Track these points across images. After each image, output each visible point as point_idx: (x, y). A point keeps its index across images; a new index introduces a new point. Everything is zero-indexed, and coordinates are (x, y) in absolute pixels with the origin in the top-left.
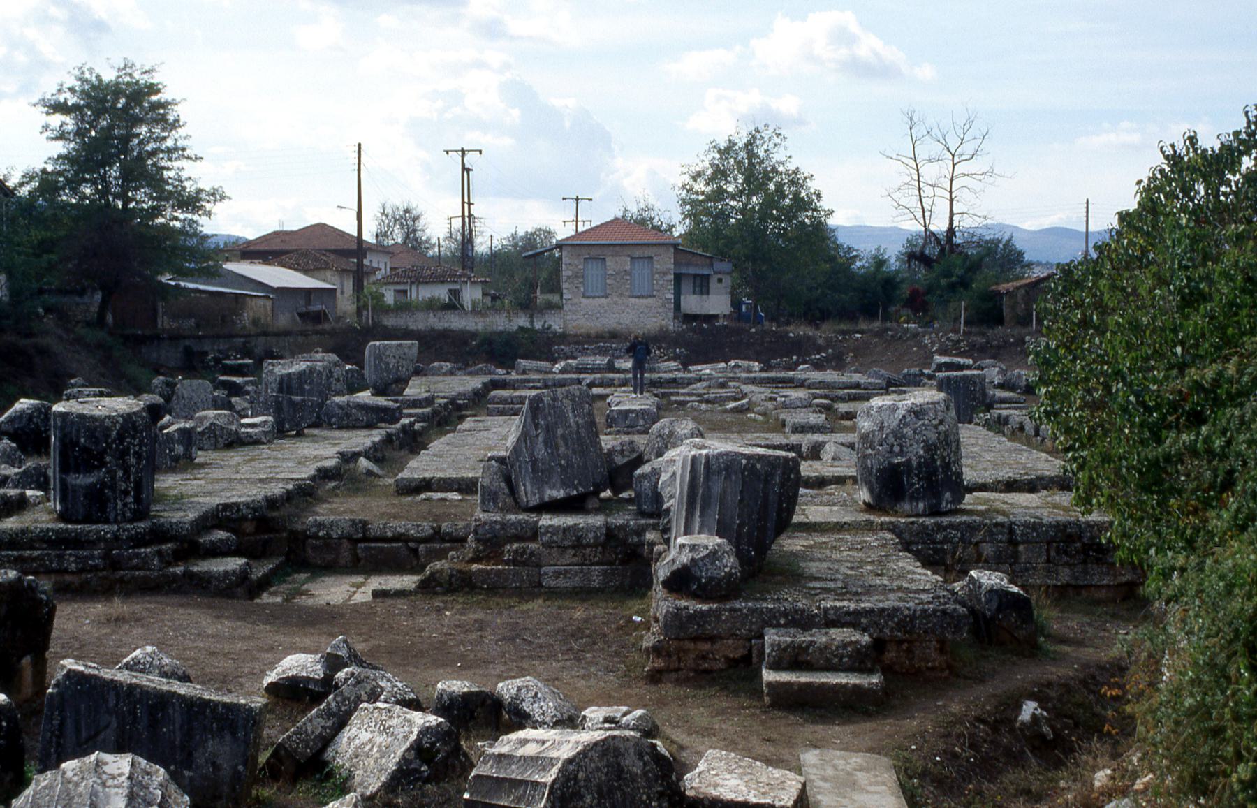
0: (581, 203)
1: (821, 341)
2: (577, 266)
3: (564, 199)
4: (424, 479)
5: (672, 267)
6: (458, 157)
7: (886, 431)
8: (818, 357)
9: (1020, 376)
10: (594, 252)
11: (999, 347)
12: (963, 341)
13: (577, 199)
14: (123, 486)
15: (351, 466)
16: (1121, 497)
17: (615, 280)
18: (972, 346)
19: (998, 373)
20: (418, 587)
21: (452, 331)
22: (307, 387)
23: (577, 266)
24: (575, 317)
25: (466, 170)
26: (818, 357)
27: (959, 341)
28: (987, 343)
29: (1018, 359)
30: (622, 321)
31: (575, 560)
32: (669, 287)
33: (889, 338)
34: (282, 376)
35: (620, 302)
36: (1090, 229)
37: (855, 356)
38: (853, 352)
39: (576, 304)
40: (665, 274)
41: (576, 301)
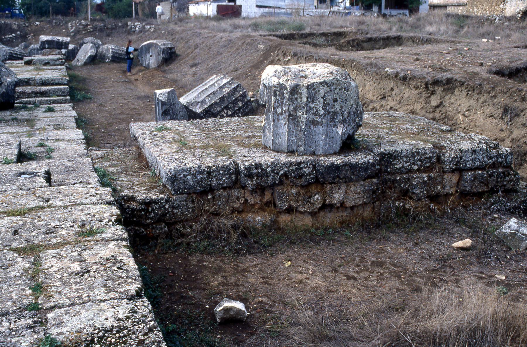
1: (15, 27)
7: (460, 89)
8: (10, 36)
9: (108, 50)
11: (112, 29)
12: (89, 25)
15: (123, 126)
16: (360, 171)
18: (95, 28)
19: (92, 48)
20: (213, 312)
21: (230, 18)
26: (10, 36)
27: (87, 25)
28: (105, 26)
29: (123, 36)
33: (54, 24)
34: (164, 49)
37: (34, 36)
38: (33, 33)
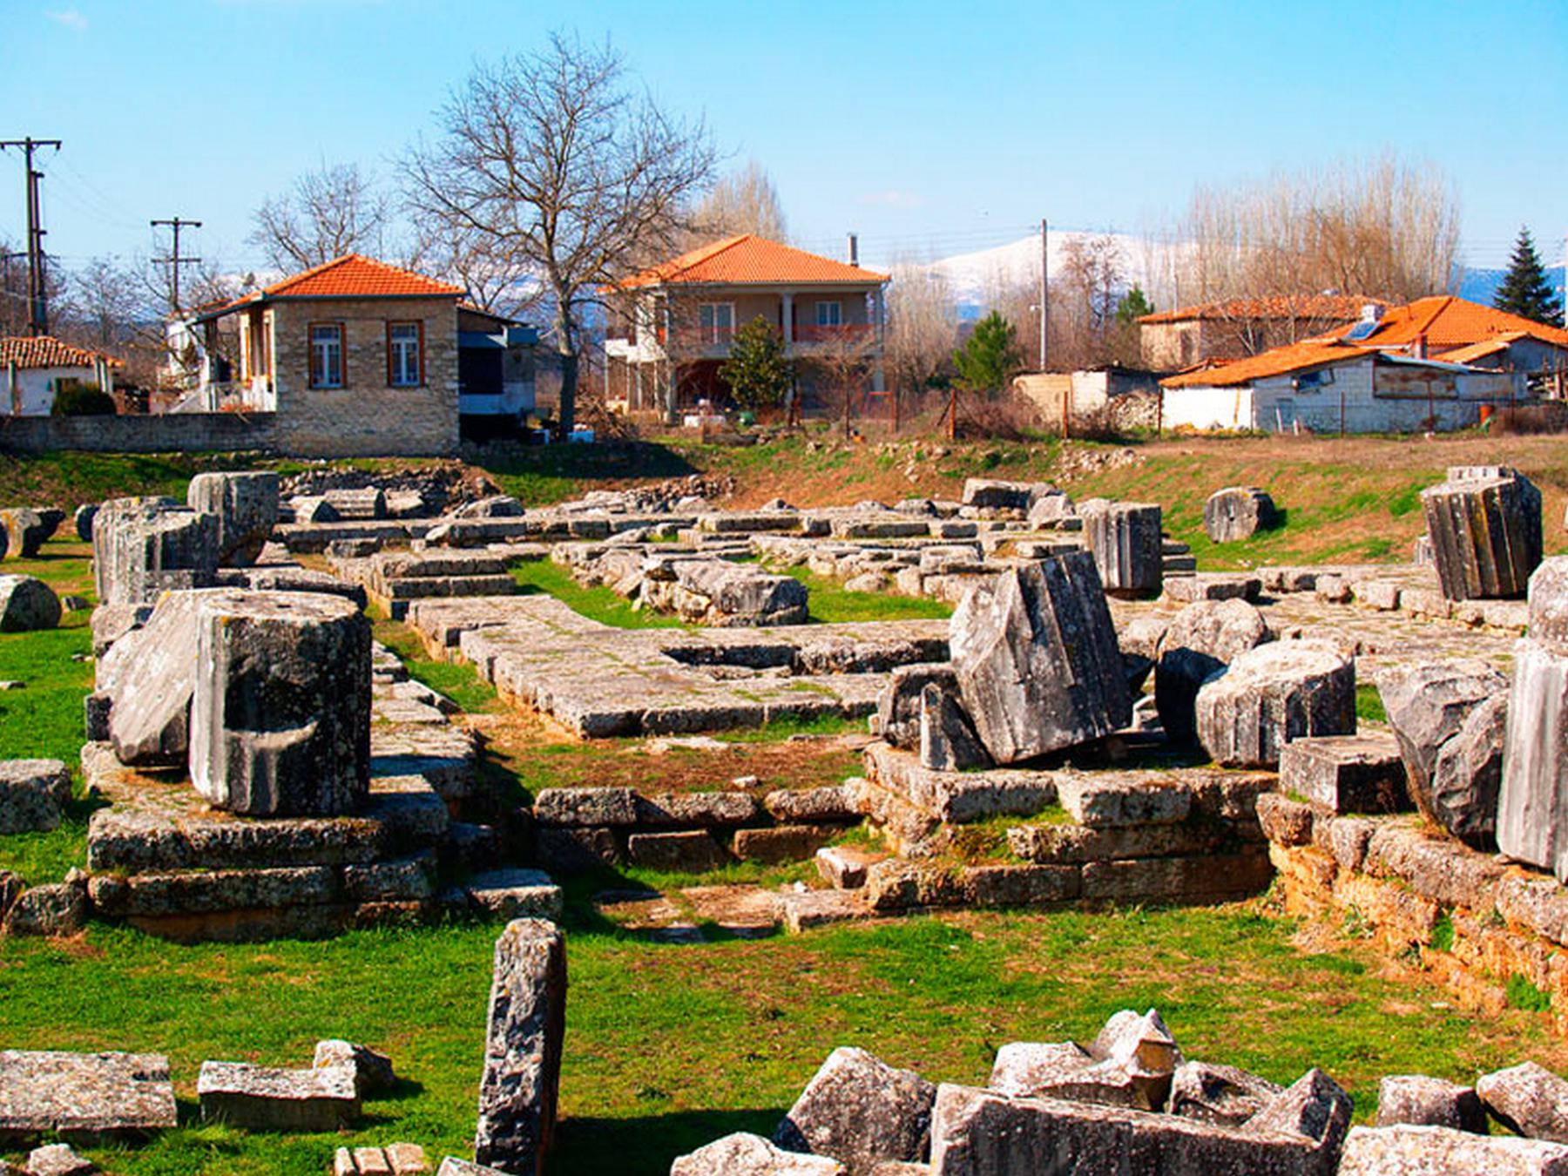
0: (183, 231)
2: (297, 337)
3: (154, 223)
4: (629, 714)
5: (455, 336)
6: (19, 153)
10: (328, 311)
13: (176, 224)
14: (342, 749)
17: (362, 360)
22: (196, 557)
23: (297, 337)
24: (295, 424)
25: (33, 176)
30: (373, 428)
31: (1137, 849)
32: (451, 371)
35: (370, 396)
36: (1049, 276)
39: (296, 402)
40: (443, 348)
41: (297, 396)
